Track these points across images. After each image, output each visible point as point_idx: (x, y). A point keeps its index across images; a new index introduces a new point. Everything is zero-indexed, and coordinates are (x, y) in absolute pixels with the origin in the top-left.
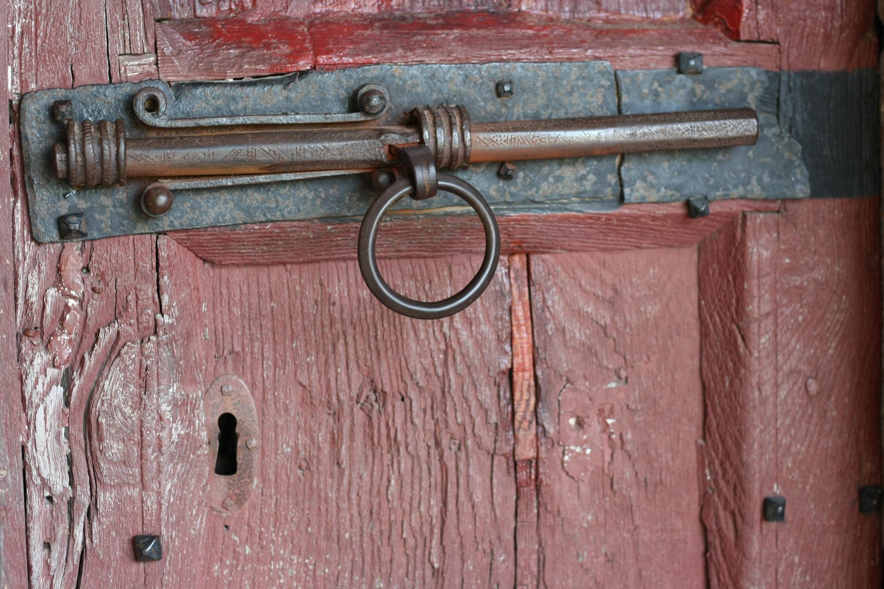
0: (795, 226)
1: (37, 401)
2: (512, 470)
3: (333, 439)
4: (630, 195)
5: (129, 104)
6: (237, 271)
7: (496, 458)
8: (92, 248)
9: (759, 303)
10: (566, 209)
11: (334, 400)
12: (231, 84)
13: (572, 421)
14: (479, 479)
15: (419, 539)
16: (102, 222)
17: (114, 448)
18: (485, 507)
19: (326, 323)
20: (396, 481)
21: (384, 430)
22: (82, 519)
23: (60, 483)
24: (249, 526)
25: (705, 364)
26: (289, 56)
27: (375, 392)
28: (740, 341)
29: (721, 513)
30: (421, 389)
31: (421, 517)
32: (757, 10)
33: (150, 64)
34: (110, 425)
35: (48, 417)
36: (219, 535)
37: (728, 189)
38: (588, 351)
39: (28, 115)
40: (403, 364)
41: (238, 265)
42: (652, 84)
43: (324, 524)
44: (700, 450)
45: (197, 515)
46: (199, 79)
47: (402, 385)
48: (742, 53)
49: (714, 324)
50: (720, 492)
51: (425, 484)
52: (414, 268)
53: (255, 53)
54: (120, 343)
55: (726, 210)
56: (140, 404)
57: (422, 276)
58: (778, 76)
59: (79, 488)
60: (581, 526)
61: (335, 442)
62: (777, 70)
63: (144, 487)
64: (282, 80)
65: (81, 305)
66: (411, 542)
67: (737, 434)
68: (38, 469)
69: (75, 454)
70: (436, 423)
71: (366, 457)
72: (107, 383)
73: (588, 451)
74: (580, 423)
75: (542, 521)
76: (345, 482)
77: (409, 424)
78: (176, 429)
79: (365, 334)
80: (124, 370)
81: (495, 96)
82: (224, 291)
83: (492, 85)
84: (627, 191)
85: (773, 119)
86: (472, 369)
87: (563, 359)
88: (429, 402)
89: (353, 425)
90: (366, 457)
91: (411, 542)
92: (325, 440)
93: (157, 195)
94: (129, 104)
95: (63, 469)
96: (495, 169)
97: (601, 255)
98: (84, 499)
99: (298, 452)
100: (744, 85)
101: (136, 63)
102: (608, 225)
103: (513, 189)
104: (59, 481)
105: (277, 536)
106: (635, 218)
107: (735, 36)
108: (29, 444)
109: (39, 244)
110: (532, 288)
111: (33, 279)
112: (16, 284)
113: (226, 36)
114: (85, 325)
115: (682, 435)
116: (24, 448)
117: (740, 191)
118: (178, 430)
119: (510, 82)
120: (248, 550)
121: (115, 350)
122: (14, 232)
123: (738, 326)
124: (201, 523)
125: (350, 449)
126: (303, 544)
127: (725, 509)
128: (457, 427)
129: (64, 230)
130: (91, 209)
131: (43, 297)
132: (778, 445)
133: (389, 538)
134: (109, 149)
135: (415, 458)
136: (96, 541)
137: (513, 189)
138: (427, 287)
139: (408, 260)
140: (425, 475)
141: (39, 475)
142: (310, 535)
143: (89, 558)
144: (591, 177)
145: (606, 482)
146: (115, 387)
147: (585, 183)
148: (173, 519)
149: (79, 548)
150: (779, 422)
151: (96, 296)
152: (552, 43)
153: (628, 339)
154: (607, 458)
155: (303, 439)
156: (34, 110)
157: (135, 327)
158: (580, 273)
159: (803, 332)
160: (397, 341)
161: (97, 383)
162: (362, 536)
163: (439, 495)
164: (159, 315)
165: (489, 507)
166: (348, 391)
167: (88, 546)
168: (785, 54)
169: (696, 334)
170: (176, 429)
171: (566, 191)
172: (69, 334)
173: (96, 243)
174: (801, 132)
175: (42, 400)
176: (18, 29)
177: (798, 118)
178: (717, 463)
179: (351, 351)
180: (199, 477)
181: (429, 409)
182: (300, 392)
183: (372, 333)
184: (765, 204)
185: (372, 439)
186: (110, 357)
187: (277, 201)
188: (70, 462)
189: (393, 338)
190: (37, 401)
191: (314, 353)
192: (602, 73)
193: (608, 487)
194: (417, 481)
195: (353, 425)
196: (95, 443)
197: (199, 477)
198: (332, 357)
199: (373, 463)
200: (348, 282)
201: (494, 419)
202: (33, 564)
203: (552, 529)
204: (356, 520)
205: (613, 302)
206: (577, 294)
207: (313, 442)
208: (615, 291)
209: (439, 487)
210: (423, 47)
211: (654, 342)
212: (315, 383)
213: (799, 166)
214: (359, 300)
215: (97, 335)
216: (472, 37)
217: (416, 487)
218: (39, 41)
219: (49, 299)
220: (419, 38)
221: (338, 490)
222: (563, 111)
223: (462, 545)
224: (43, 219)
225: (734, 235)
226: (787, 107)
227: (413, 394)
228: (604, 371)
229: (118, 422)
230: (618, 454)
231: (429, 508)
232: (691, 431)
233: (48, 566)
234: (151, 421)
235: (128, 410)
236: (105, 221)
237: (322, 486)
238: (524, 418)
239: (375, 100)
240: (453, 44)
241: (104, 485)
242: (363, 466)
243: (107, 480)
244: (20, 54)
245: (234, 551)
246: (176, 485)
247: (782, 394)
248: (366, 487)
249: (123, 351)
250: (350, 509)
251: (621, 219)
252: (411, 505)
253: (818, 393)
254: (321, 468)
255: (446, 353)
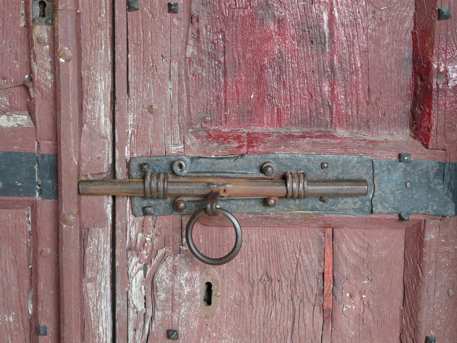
0: (448, 227)
1: (133, 275)
2: (322, 312)
3: (250, 294)
4: (375, 211)
5: (172, 164)
6: (215, 228)
7: (316, 307)
8: (156, 219)
9: (429, 256)
10: (348, 214)
11: (251, 280)
12: (214, 158)
13: (348, 295)
14: (308, 315)
15: (282, 335)
16: (160, 209)
17: (162, 296)
18: (310, 326)
19: (249, 250)
20: (274, 313)
21: (270, 292)
22: (149, 321)
23: (141, 307)
24: (215, 325)
25: (405, 277)
26: (237, 147)
27: (268, 277)
28: (420, 271)
29: (408, 338)
30: (286, 278)
31: (284, 327)
32: (437, 137)
33: (181, 149)
34: (161, 287)
35: (137, 282)
36: (204, 328)
37: (418, 210)
38: (356, 268)
39: (132, 167)
40: (280, 268)
41: (216, 226)
42: (388, 166)
43: (245, 327)
44: (401, 311)
45: (194, 321)
46: (200, 155)
47: (279, 276)
48: (429, 154)
49: (410, 262)
50: (408, 330)
51: (286, 315)
52: (286, 231)
53: (223, 146)
54: (166, 256)
55: (417, 218)
56: (172, 279)
57: (289, 234)
58: (444, 164)
59: (148, 309)
60: (349, 337)
61: (251, 295)
62: (444, 161)
63: (173, 311)
64: (234, 157)
65: (151, 240)
66: (279, 337)
67: (417, 309)
68: (132, 301)
69: (147, 296)
70: (292, 291)
71: (263, 302)
72: (160, 270)
73: (354, 307)
74: (351, 296)
75: (333, 333)
76: (254, 311)
77: (281, 290)
78: (187, 289)
79: (265, 255)
80: (167, 266)
81: (321, 168)
82: (210, 235)
83: (320, 164)
84: (374, 209)
85: (441, 181)
86: (308, 272)
87: (344, 270)
88: (289, 283)
89: (258, 290)
90: (263, 302)
91: (279, 337)
92: (247, 295)
93: (180, 204)
94: (172, 164)
95: (142, 302)
96: (319, 198)
97: (364, 230)
98: (150, 314)
99: (236, 299)
100: (429, 168)
101: (176, 148)
102: (366, 221)
103: (326, 206)
104: (140, 306)
105: (226, 330)
106: (378, 219)
107: (426, 147)
108: (129, 292)
109: (135, 216)
110: (334, 242)
111: (133, 229)
112: (126, 230)
113: (213, 137)
114: (152, 248)
115: (394, 304)
116: (127, 293)
117: (424, 211)
118: (187, 290)
119: (327, 163)
120: (214, 334)
121: (164, 258)
122: (126, 210)
123: (419, 265)
124: (196, 324)
125: (257, 299)
126: (236, 334)
127: (410, 337)
128: (300, 294)
129: (145, 213)
130: (156, 204)
131: (136, 236)
132: (434, 315)
133: (270, 335)
134: (161, 185)
135: (283, 304)
136: (153, 330)
137: (326, 206)
138: (291, 238)
139: (284, 228)
140: (286, 311)
141: (133, 303)
142: (239, 331)
143: (150, 336)
144: (360, 203)
145: (360, 319)
146: (163, 272)
147: (356, 204)
148: (184, 324)
149: (147, 332)
150: (435, 306)
151: (157, 237)
152: (347, 146)
153: (373, 264)
154: (362, 310)
155: (238, 294)
156: (134, 166)
157: (172, 250)
158: (355, 238)
159: (448, 270)
160: (277, 258)
161: (157, 270)
162: (260, 332)
163: (292, 319)
164: (181, 246)
165: (312, 325)
166: (256, 276)
167: (151, 332)
168: (448, 155)
169: (402, 264)
170: (187, 289)
171: (348, 207)
172: (146, 251)
173: (158, 217)
174: (453, 188)
175: (135, 275)
176: (130, 132)
177: (452, 182)
178: (408, 318)
179: (259, 261)
180: (196, 306)
181: (289, 285)
182: (238, 276)
183: (268, 255)
184: (435, 216)
185: (266, 295)
186: (162, 260)
187: (229, 205)
188: (145, 298)
189: (276, 257)
190: (133, 275)
191: (244, 260)
192: (367, 161)
193: (362, 322)
194: (283, 313)
195: (258, 290)
196: (155, 293)
197: (196, 306)
198: (251, 263)
199: (266, 305)
200: (259, 235)
201: (315, 292)
202: (129, 337)
203: (337, 337)
204: (258, 327)
205: (368, 249)
206: (352, 245)
207: (242, 295)
208: (369, 245)
209: (292, 316)
210: (292, 146)
211: (384, 266)
212: (244, 273)
213: (451, 202)
214: (263, 242)
215: (157, 252)
216: (314, 142)
217: (282, 315)
218: (138, 137)
219: (139, 238)
220: (291, 142)
221: (251, 314)
222: (349, 175)
223: (300, 339)
224: (137, 207)
225: (420, 228)
226: (447, 178)
227: (283, 279)
228: (362, 276)
229: (164, 286)
230: (366, 309)
231: (287, 324)
232: (398, 302)
233: (134, 338)
234: (177, 286)
235: (168, 282)
236: (161, 209)
237: (245, 312)
238: (328, 292)
239: (270, 169)
240: (305, 145)
241: (158, 310)
242: (262, 305)
243: (158, 307)
244: (131, 142)
245: (209, 334)
246: (186, 311)
247: (437, 295)
248: (263, 314)
249: (167, 259)
250: (255, 322)
251: (372, 219)
252: (280, 322)
253: (453, 296)
254: (245, 305)
255: (297, 264)
